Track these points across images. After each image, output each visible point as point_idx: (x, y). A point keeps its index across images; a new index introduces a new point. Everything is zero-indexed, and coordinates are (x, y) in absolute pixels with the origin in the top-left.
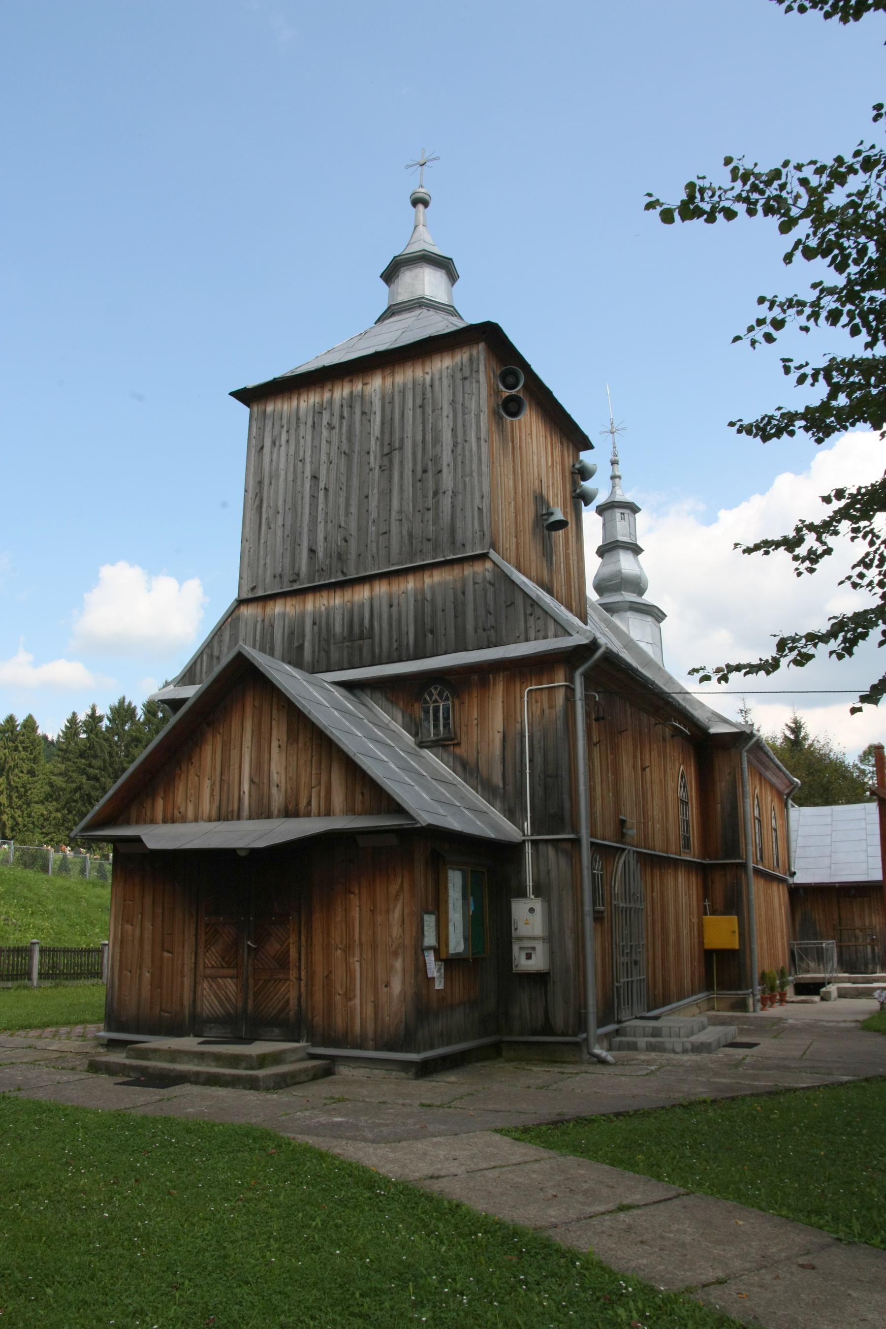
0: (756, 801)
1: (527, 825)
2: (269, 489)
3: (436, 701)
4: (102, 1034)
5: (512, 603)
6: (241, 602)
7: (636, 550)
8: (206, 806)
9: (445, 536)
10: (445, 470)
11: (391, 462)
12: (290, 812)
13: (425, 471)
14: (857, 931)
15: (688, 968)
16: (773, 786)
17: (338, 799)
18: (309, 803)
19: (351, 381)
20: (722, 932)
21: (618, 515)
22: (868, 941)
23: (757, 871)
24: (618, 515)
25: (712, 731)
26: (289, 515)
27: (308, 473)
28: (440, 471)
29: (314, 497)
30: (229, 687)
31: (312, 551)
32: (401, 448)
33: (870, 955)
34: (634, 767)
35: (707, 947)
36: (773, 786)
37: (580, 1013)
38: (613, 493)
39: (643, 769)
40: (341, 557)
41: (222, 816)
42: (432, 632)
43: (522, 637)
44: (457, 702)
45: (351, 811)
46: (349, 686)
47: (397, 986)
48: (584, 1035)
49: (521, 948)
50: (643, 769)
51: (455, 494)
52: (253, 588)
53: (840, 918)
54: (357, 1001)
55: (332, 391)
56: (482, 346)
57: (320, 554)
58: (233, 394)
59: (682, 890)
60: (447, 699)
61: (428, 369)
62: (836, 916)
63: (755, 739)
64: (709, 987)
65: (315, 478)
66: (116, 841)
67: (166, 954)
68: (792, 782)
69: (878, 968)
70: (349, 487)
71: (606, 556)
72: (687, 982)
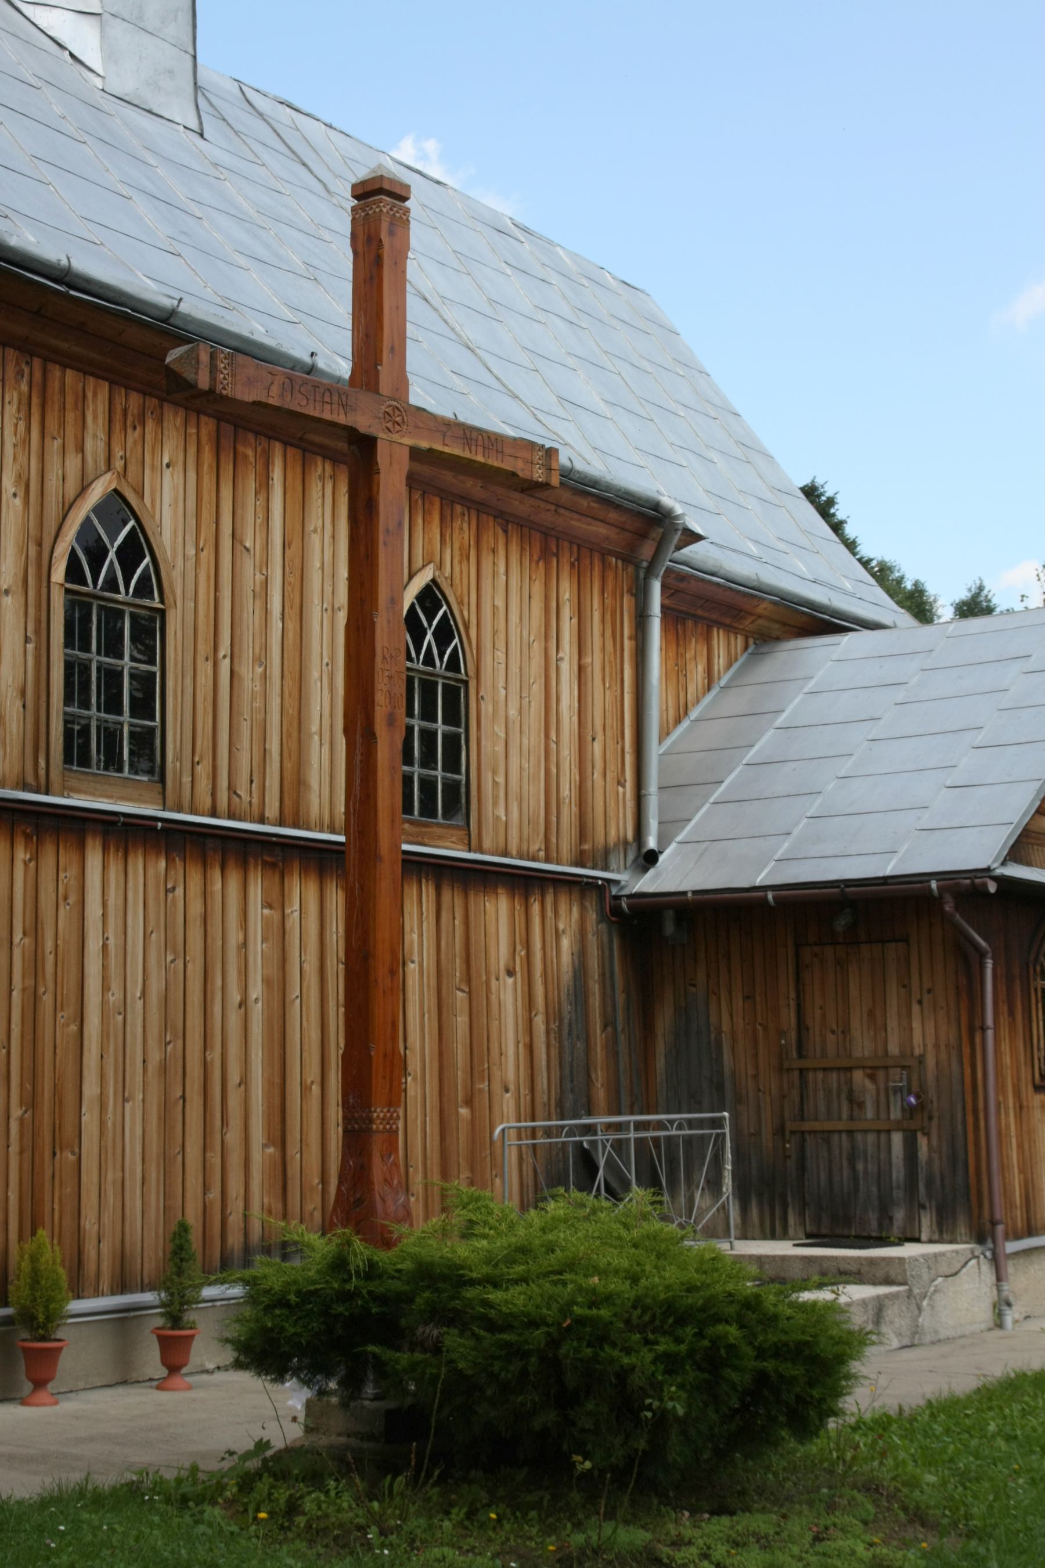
14: (858, 1076)
22: (896, 1114)
33: (898, 1171)
42: (469, 1102)
53: (802, 1026)
56: (295, 1432)
62: (788, 1017)
63: (667, 602)
69: (927, 1223)
70: (618, 818)
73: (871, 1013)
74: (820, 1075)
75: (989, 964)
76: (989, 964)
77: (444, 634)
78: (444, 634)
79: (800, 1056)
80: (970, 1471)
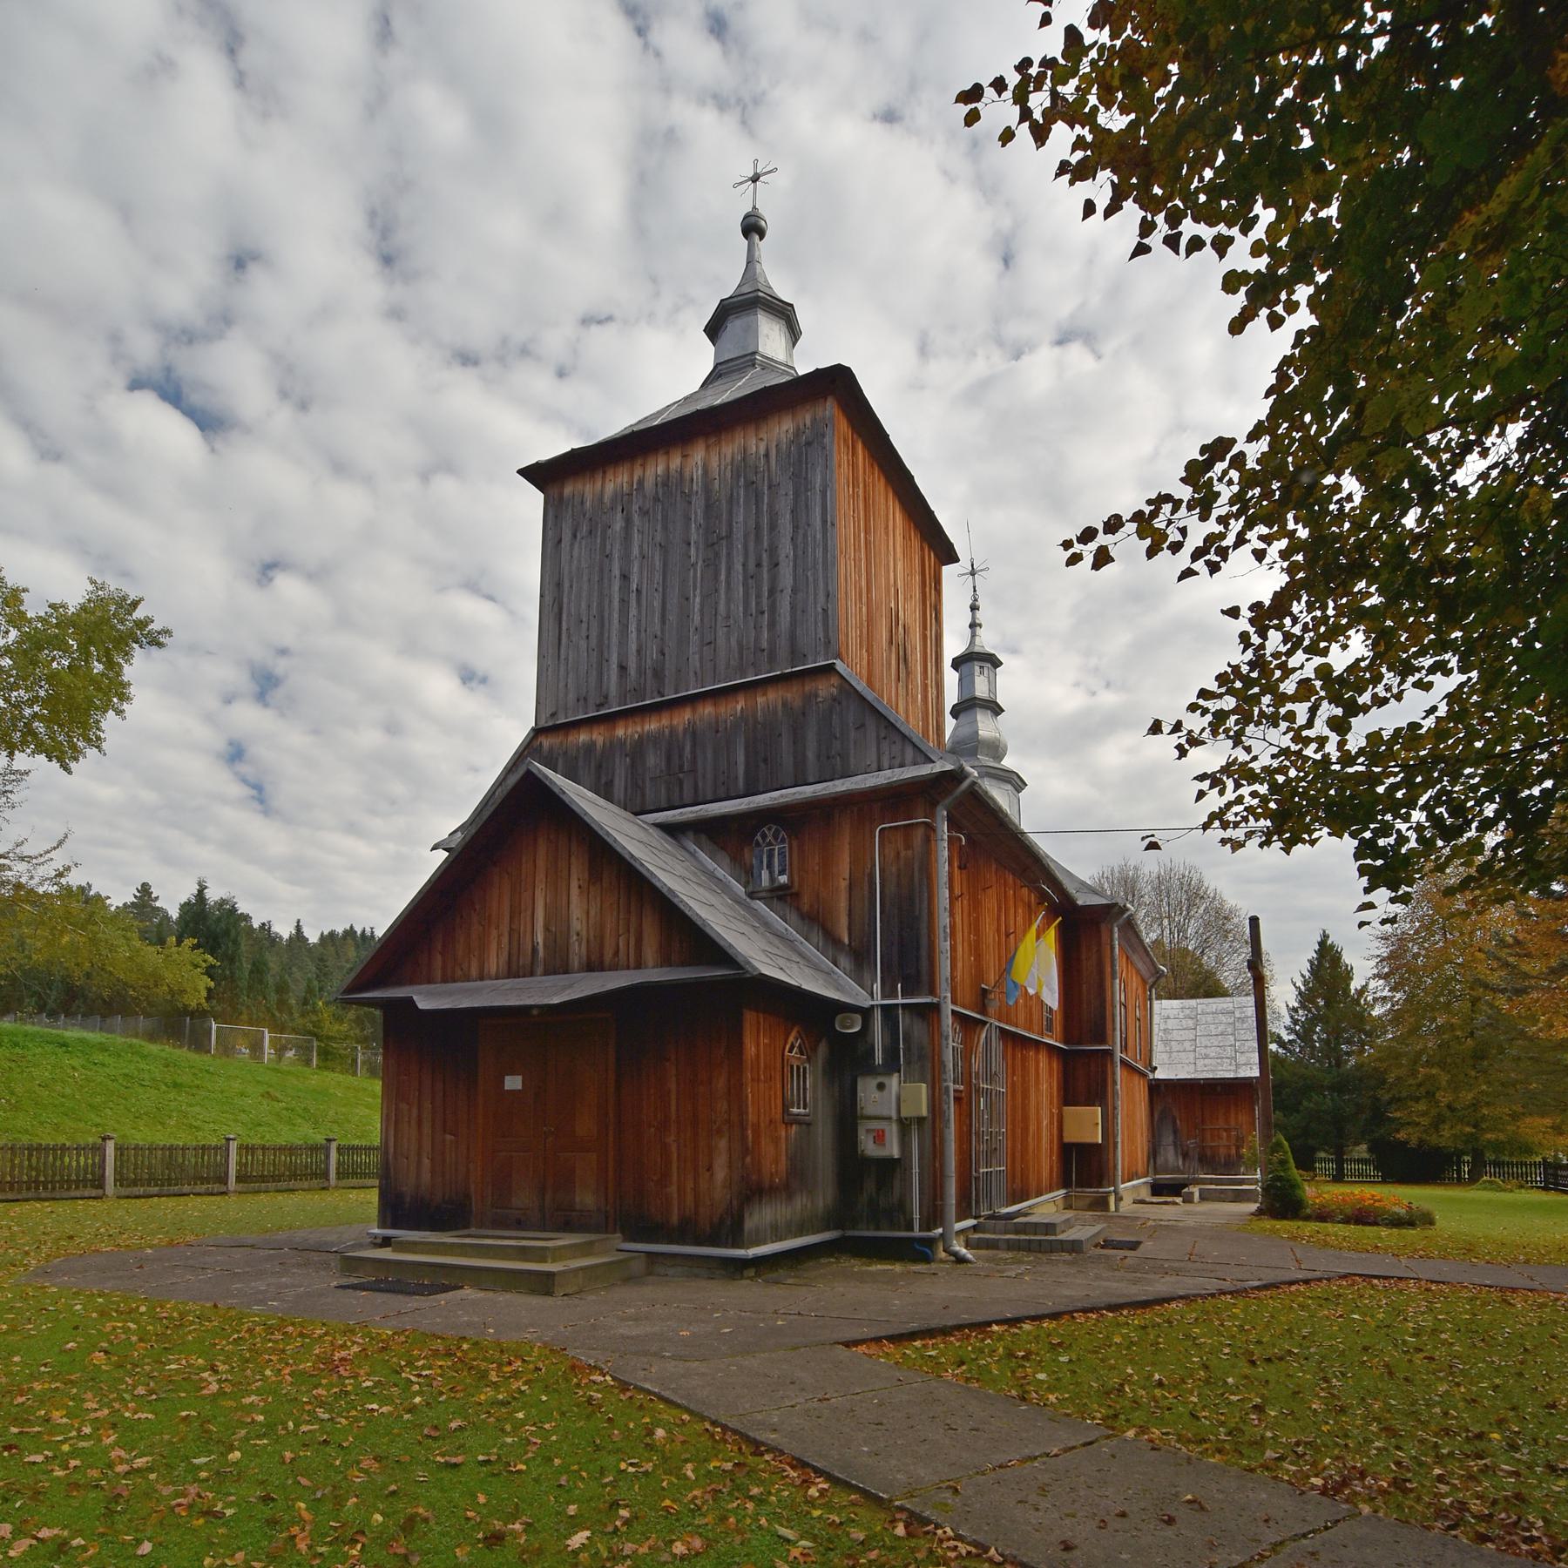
0: (1122, 988)
1: (877, 987)
2: (570, 593)
3: (770, 844)
4: (376, 1231)
5: (863, 725)
6: (537, 732)
7: (996, 710)
8: (494, 963)
9: (783, 643)
10: (783, 564)
11: (717, 555)
12: (593, 965)
13: (759, 565)
15: (1045, 1161)
16: (1138, 971)
17: (650, 953)
18: (617, 953)
19: (667, 453)
20: (1086, 1124)
21: (977, 669)
23: (1123, 1061)
24: (977, 669)
25: (1080, 903)
26: (595, 624)
27: (616, 572)
28: (777, 565)
29: (624, 602)
30: (517, 822)
31: (623, 668)
32: (729, 536)
34: (998, 930)
35: (1066, 1140)
36: (1138, 971)
37: (935, 1206)
38: (972, 642)
39: (1007, 936)
40: (658, 674)
41: (512, 972)
43: (874, 766)
44: (795, 844)
45: (665, 961)
46: (671, 830)
47: (720, 1174)
48: (940, 1230)
49: (868, 1131)
50: (1007, 936)
51: (795, 591)
52: (553, 715)
54: (674, 1188)
55: (643, 466)
57: (632, 671)
58: (524, 472)
59: (1045, 1078)
60: (783, 841)
61: (764, 436)
64: (1066, 1183)
65: (625, 577)
66: (388, 1006)
67: (448, 1137)
68: (1158, 971)
71: (961, 717)
72: (1045, 1174)
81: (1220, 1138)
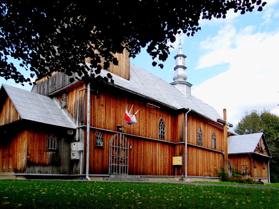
73: (243, 162)
74: (239, 166)
75: (252, 159)
76: (252, 159)
77: (163, 123)
78: (163, 123)
79: (237, 165)
80: (271, 204)
81: (241, 168)
